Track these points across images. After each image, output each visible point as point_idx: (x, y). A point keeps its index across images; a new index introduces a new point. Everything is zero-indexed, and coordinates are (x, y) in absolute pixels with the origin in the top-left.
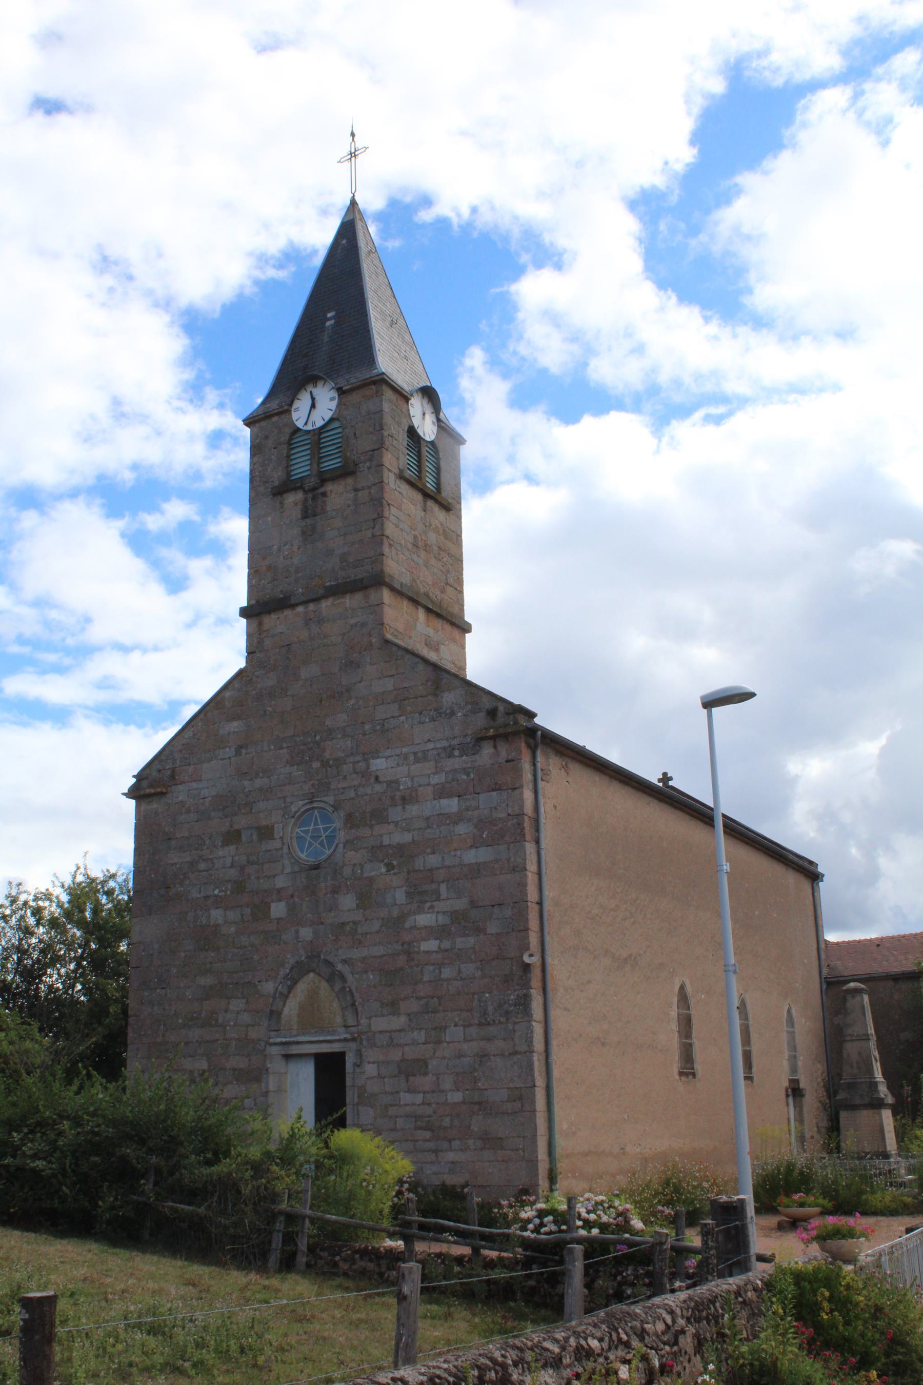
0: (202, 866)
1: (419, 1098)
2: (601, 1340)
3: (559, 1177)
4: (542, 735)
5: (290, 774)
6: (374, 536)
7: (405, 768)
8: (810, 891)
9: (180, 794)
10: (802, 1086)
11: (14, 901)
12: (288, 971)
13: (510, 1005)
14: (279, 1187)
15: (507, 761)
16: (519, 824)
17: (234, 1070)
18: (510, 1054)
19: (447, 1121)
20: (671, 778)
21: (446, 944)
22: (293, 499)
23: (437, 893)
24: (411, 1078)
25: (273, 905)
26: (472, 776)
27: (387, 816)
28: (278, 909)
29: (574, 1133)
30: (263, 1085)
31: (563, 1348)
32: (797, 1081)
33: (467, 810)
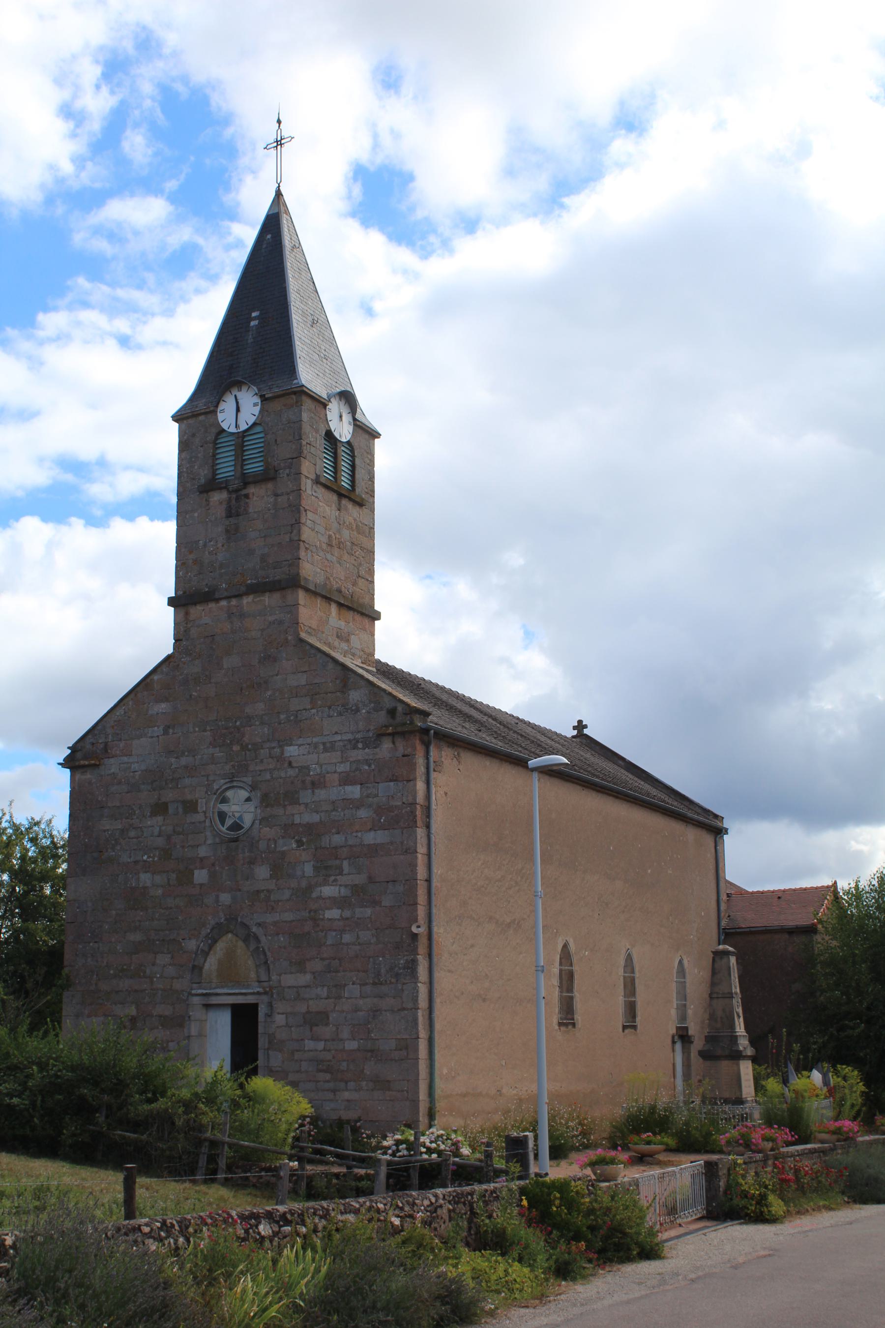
0: (132, 834)
1: (321, 1045)
2: (385, 1205)
5: (213, 754)
6: (291, 540)
7: (315, 756)
8: (712, 844)
9: (112, 766)
10: (690, 1032)
13: (400, 969)
14: (205, 1120)
15: (403, 756)
17: (160, 1016)
18: (399, 1010)
20: (586, 727)
21: (347, 913)
22: (218, 497)
24: (315, 1028)
25: (196, 872)
26: (373, 767)
27: (298, 798)
28: (201, 876)
29: (454, 1077)
30: (186, 1031)
31: (361, 1206)
32: (686, 1028)
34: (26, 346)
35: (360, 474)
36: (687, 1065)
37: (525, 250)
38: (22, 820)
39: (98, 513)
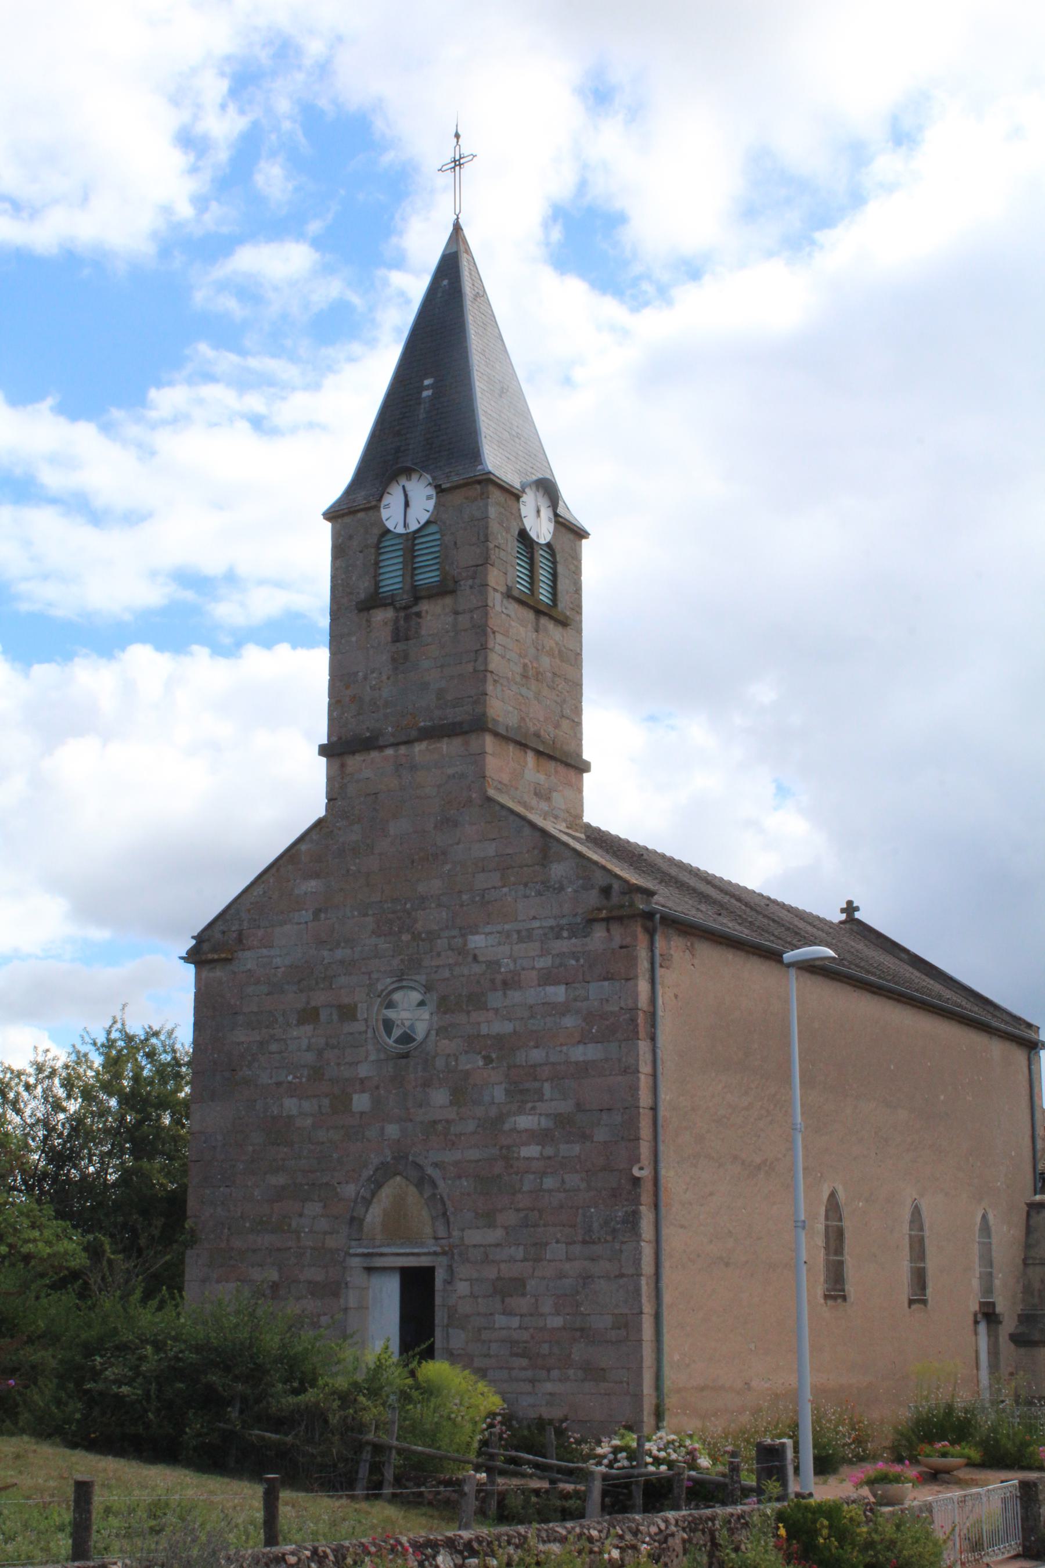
0: (274, 1047)
1: (515, 1322)
2: (600, 1531)
3: (667, 1413)
4: (661, 917)
5: (376, 945)
6: (475, 671)
8: (1025, 1063)
9: (248, 960)
10: (999, 1309)
11: (40, 1068)
12: (371, 1173)
13: (618, 1223)
14: (367, 1417)
15: (621, 947)
16: (632, 1020)
17: (310, 1282)
18: (616, 1277)
19: (545, 1348)
20: (857, 909)
21: (549, 1151)
22: (382, 616)
23: (540, 1092)
25: (355, 1097)
26: (582, 961)
28: (361, 1102)
29: (688, 1365)
30: (342, 1301)
31: (569, 1532)
33: (575, 1000)
34: (134, 431)
35: (563, 584)
36: (994, 1352)
37: (766, 298)
38: (136, 1029)
39: (227, 640)
